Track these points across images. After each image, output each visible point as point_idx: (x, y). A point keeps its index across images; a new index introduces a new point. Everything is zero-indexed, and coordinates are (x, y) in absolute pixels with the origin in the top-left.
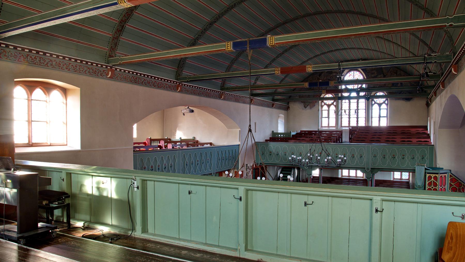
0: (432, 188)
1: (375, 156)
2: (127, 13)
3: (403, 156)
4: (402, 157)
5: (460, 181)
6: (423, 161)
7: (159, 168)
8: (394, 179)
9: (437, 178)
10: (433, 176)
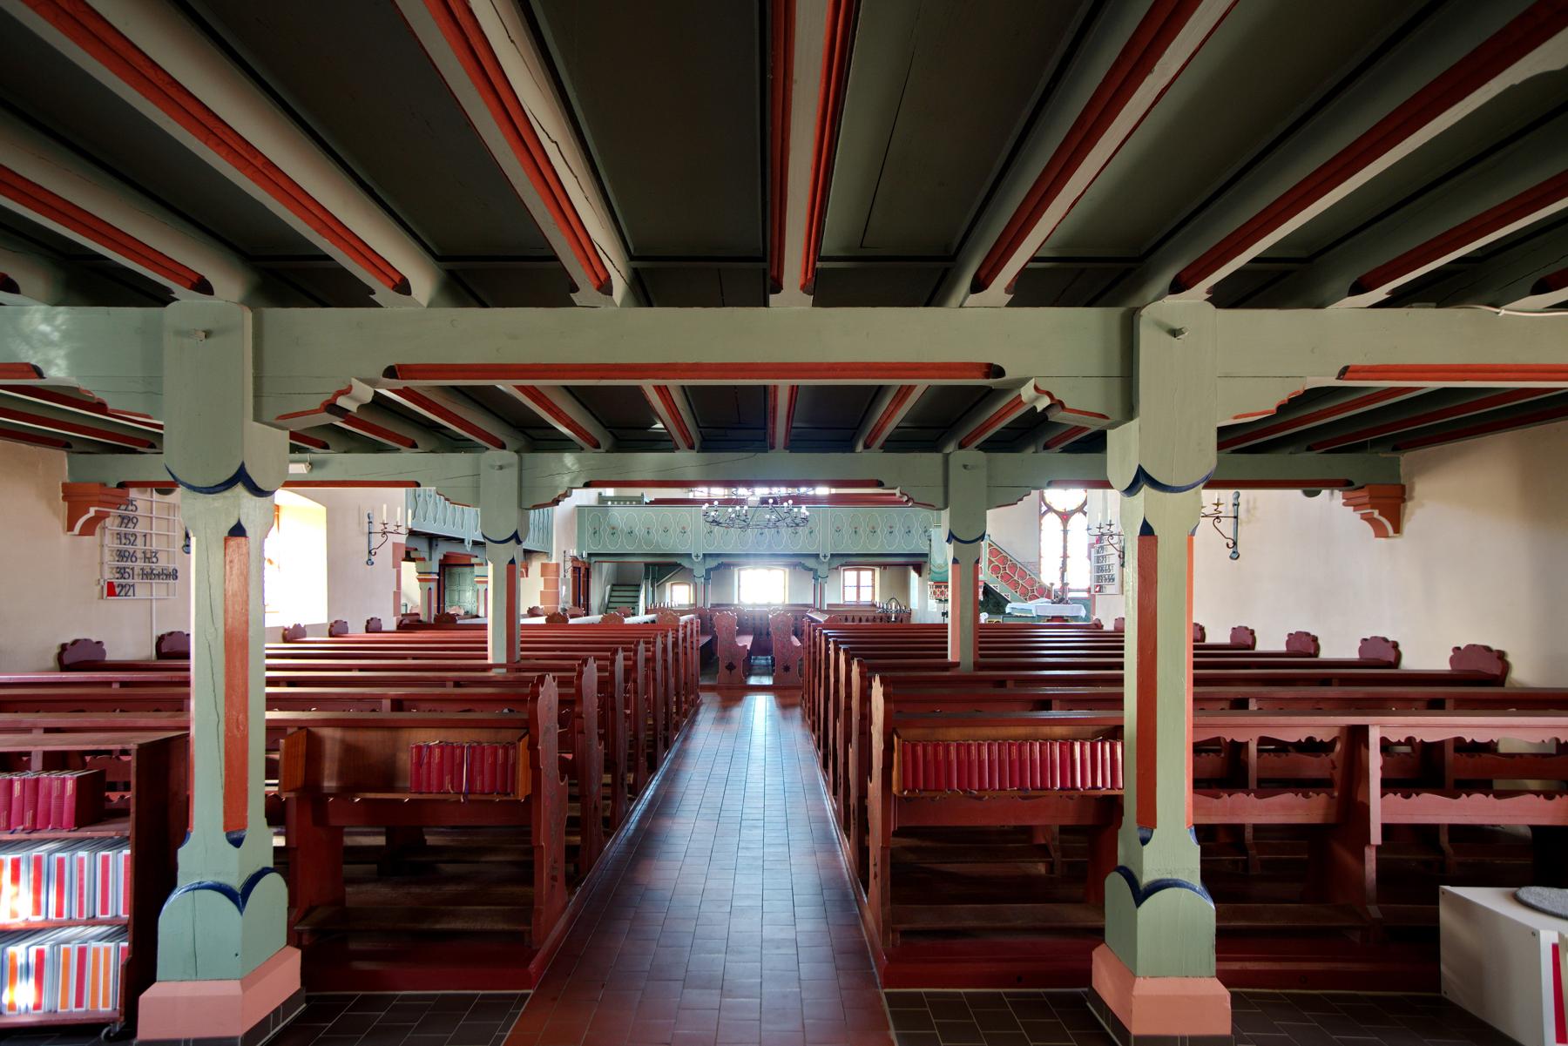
1: (838, 530)
3: (891, 527)
4: (890, 530)
5: (1005, 554)
8: (873, 570)
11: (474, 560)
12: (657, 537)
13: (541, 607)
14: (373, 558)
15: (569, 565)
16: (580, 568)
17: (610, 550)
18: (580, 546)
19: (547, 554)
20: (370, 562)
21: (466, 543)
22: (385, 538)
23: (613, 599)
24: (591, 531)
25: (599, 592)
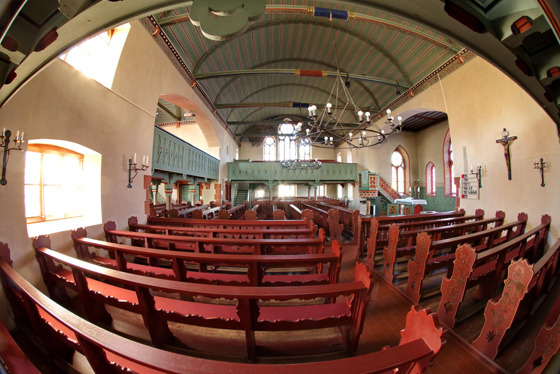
0: (373, 185)
3: (340, 171)
4: (339, 171)
7: (172, 154)
8: (324, 185)
9: (375, 178)
10: (373, 176)
11: (189, 183)
12: (256, 174)
13: (215, 201)
14: (131, 184)
15: (224, 184)
16: (228, 185)
17: (339, 179)
18: (228, 177)
19: (217, 180)
20: (130, 186)
21: (184, 176)
22: (136, 172)
23: (238, 196)
24: (232, 172)
25: (234, 194)
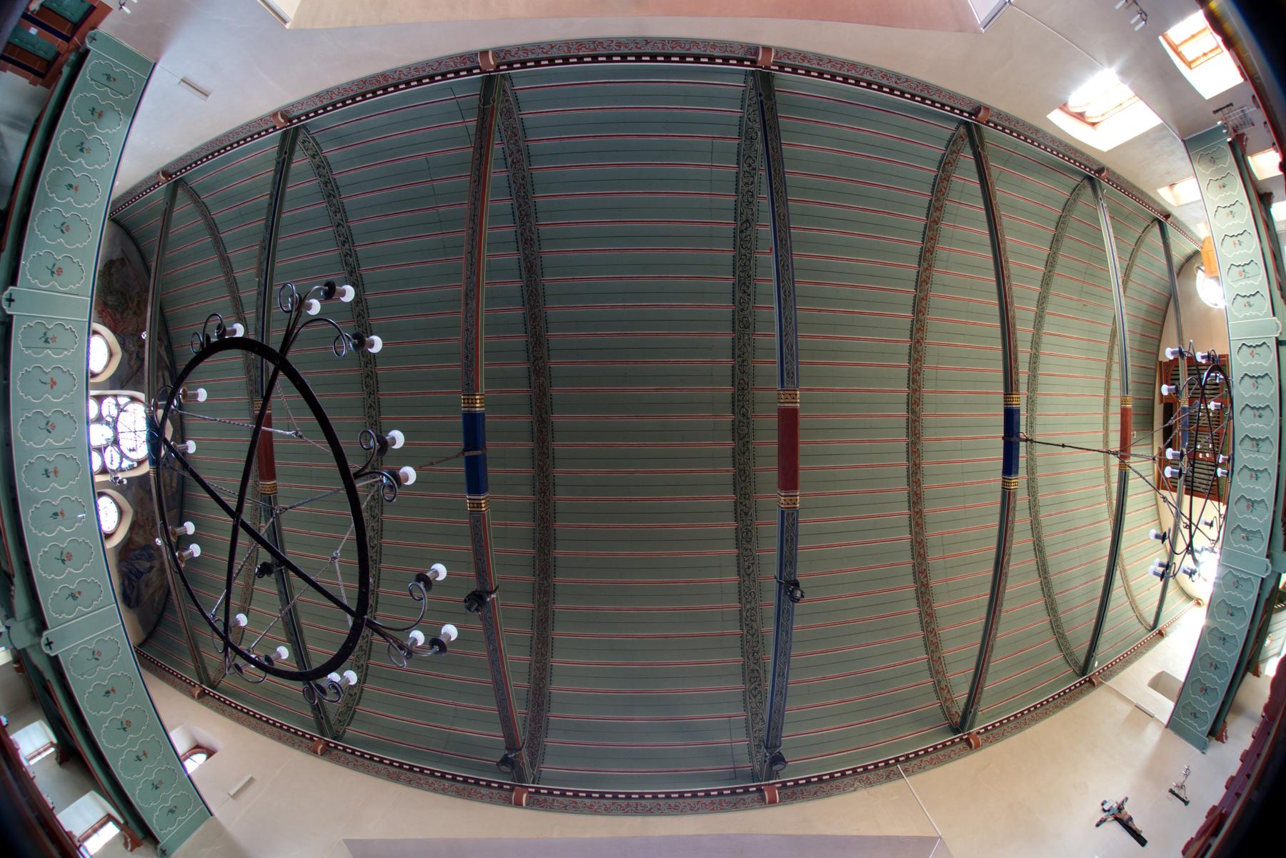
2: (943, 194)
3: (145, 754)
4: (140, 754)
6: (167, 815)
